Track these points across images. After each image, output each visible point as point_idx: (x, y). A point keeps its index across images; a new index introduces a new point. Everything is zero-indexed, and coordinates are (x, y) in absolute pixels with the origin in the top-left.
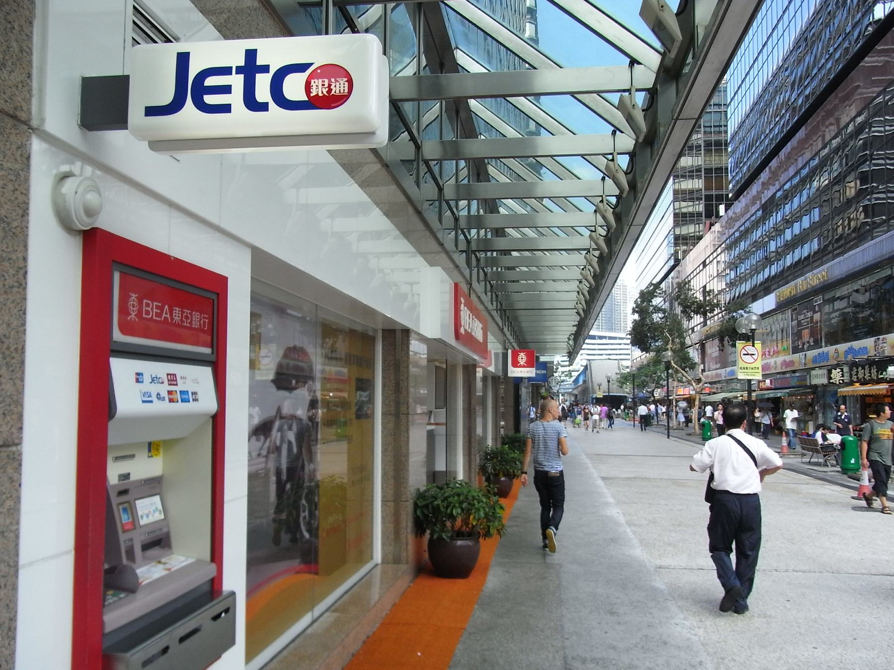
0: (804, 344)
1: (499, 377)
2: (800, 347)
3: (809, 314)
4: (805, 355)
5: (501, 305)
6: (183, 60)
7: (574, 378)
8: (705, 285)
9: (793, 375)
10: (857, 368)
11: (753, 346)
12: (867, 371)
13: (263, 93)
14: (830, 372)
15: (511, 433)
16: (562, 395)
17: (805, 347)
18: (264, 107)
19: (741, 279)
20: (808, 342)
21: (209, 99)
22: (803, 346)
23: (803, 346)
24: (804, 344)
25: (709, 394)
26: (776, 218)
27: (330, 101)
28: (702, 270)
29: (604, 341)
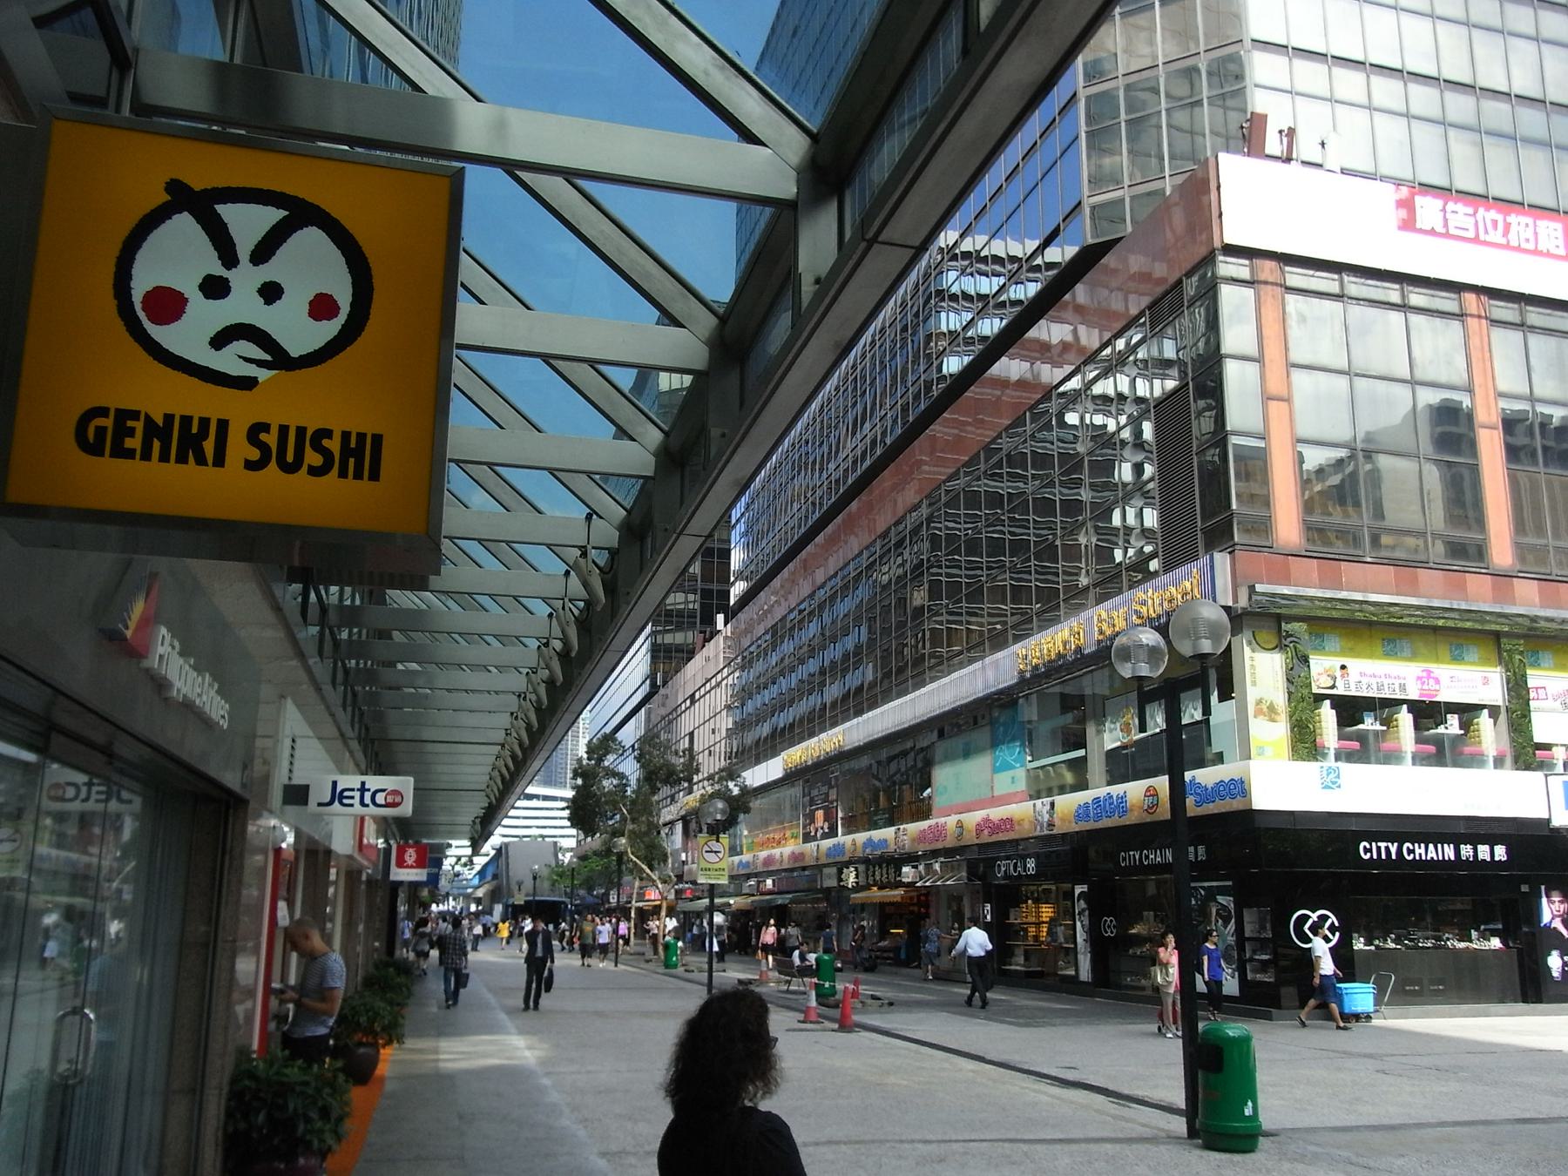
0: (817, 830)
1: (377, 881)
2: (813, 834)
3: (824, 789)
4: (1052, 805)
5: (367, 729)
6: (335, 784)
7: (478, 868)
8: (693, 732)
9: (802, 873)
10: (874, 867)
11: (718, 841)
12: (884, 871)
13: (367, 800)
14: (840, 872)
15: (385, 958)
16: (454, 899)
17: (818, 835)
18: (367, 806)
19: (759, 718)
20: (822, 828)
21: (345, 801)
22: (816, 833)
23: (816, 833)
24: (817, 830)
25: (691, 900)
26: (787, 647)
27: (394, 805)
28: (689, 708)
29: (534, 803)
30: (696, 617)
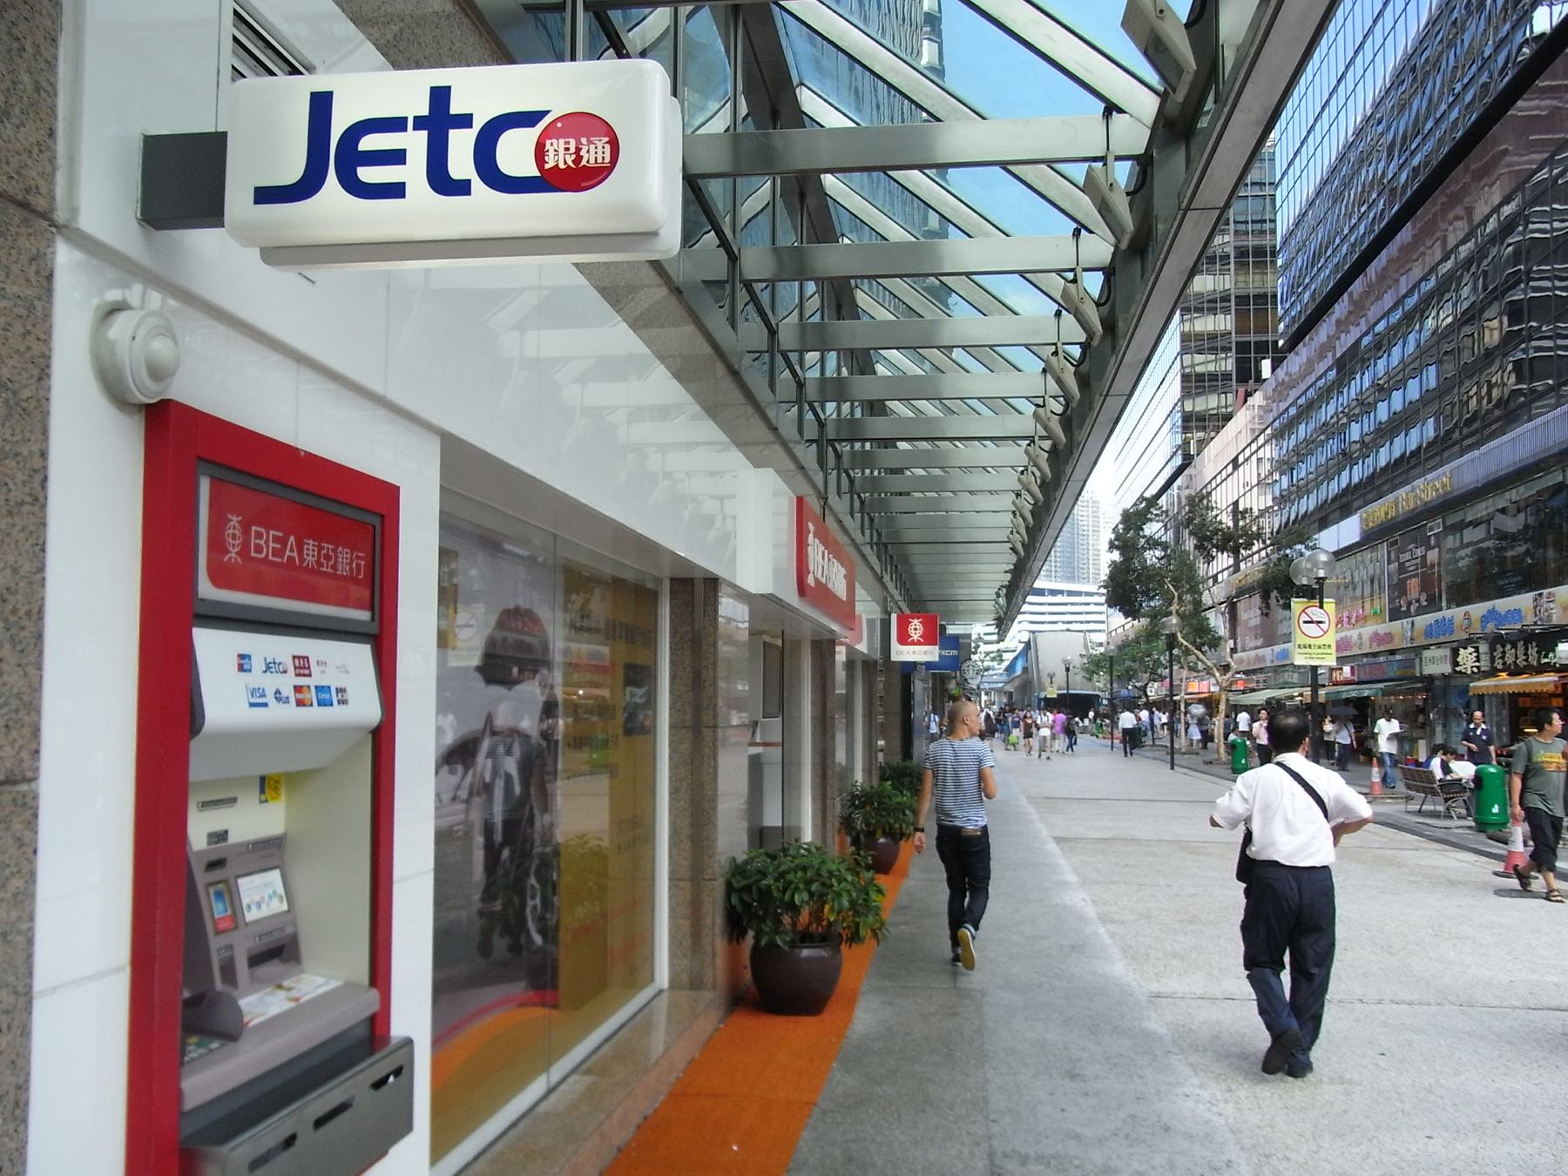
0: (1410, 604)
1: (876, 662)
2: (1404, 609)
3: (1419, 552)
4: (1413, 623)
5: (879, 534)
6: (321, 105)
7: (1006, 663)
8: (1237, 501)
9: (1391, 658)
10: (1504, 647)
11: (1321, 607)
12: (1521, 651)
13: (461, 163)
14: (1455, 653)
15: (897, 760)
16: (987, 694)
17: (1412, 609)
18: (463, 188)
19: (1300, 491)
20: (1418, 601)
21: (367, 174)
22: (1409, 608)
23: (1409, 608)
24: (1410, 604)
25: (1244, 692)
26: (1361, 382)
27: (579, 178)
28: (1231, 474)
29: (1059, 599)
30: (1231, 380)
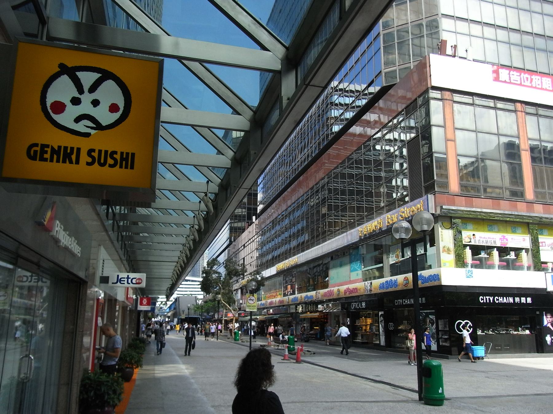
0: (288, 292)
1: (133, 310)
2: (287, 294)
3: (291, 278)
5: (129, 257)
6: (118, 276)
7: (168, 306)
8: (244, 258)
9: (283, 307)
10: (308, 305)
11: (253, 296)
12: (312, 307)
13: (130, 282)
14: (296, 307)
15: (136, 337)
16: (160, 317)
17: (289, 294)
18: (130, 284)
19: (268, 253)
20: (290, 292)
21: (122, 282)
22: (288, 293)
23: (288, 293)
24: (288, 292)
25: (244, 317)
26: (278, 228)
27: (139, 283)
28: (243, 249)
29: (188, 283)
30: (245, 217)
